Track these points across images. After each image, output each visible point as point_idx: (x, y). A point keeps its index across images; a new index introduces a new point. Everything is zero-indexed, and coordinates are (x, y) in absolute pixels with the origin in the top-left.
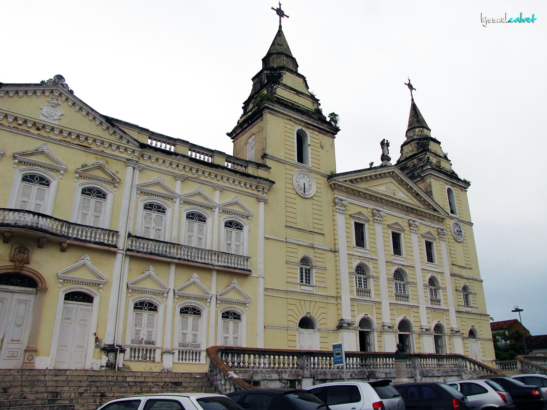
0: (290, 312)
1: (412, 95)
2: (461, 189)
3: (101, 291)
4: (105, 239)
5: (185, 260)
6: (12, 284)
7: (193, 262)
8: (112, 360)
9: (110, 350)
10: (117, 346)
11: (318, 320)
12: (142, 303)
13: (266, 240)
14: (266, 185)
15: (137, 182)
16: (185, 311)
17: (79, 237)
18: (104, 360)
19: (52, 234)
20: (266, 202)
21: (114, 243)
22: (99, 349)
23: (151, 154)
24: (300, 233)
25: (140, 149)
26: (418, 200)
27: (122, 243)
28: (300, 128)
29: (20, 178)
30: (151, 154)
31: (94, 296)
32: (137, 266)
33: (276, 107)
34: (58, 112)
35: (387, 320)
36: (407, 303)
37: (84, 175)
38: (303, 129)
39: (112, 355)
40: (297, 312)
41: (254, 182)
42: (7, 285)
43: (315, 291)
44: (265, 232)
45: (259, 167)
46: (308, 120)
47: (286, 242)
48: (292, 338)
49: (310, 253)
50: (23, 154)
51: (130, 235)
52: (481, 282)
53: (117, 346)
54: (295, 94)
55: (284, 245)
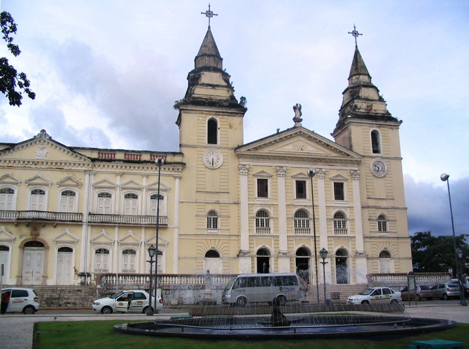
0: (199, 248)
1: (356, 42)
2: (390, 128)
3: (76, 246)
4: (76, 218)
5: (123, 223)
6: (33, 246)
7: (128, 224)
8: (83, 281)
9: (82, 275)
10: (86, 273)
11: (392, 252)
12: (100, 250)
13: (181, 204)
14: (180, 167)
15: (93, 182)
16: (125, 252)
17: (62, 219)
18: (80, 280)
19: (47, 220)
20: (180, 178)
21: (80, 220)
22: (77, 275)
23: (99, 164)
24: (208, 195)
25: (92, 163)
26: (329, 149)
28: (211, 117)
29: (30, 193)
30: (99, 164)
31: (72, 248)
32: (95, 230)
33: (189, 107)
34: (45, 151)
35: (283, 248)
36: (346, 235)
37: (61, 185)
38: (214, 117)
39: (83, 278)
41: (171, 167)
42: (31, 247)
43: (220, 233)
44: (179, 199)
45: (175, 155)
46: (217, 109)
47: (196, 202)
48: (200, 264)
49: (216, 208)
50: (30, 180)
51: (90, 214)
52: (405, 210)
53: (86, 273)
54: (211, 89)
55: (195, 204)
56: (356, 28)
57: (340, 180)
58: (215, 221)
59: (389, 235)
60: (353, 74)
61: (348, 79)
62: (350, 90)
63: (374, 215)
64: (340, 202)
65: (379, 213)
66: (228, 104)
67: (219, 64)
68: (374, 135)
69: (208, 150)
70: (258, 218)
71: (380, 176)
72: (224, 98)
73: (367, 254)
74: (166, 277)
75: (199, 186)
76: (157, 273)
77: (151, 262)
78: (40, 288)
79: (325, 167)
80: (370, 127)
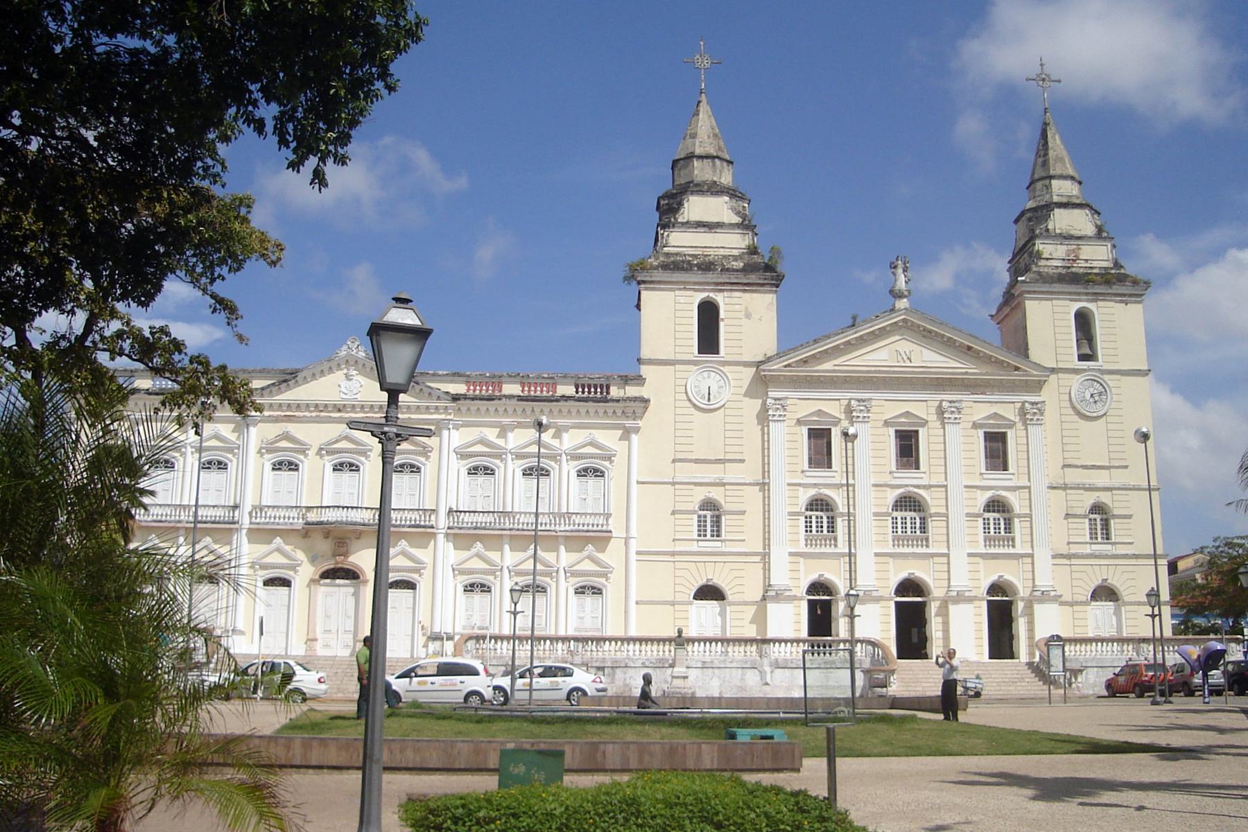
2: (1121, 302)
27: (442, 521)
31: (290, 579)
36: (1012, 551)
38: (712, 295)
39: (438, 643)
40: (690, 578)
49: (716, 494)
56: (1044, 67)
57: (999, 426)
58: (717, 522)
59: (1121, 550)
60: (1036, 176)
61: (1027, 188)
62: (1028, 215)
63: (1080, 504)
64: (911, 473)
65: (1090, 499)
66: (742, 264)
67: (723, 174)
68: (1084, 323)
69: (699, 369)
70: (809, 513)
71: (1095, 415)
72: (735, 252)
73: (1059, 594)
74: (711, 643)
75: (678, 448)
76: (536, 633)
77: (1153, 616)
78: (347, 663)
79: (966, 398)
80: (1071, 300)
